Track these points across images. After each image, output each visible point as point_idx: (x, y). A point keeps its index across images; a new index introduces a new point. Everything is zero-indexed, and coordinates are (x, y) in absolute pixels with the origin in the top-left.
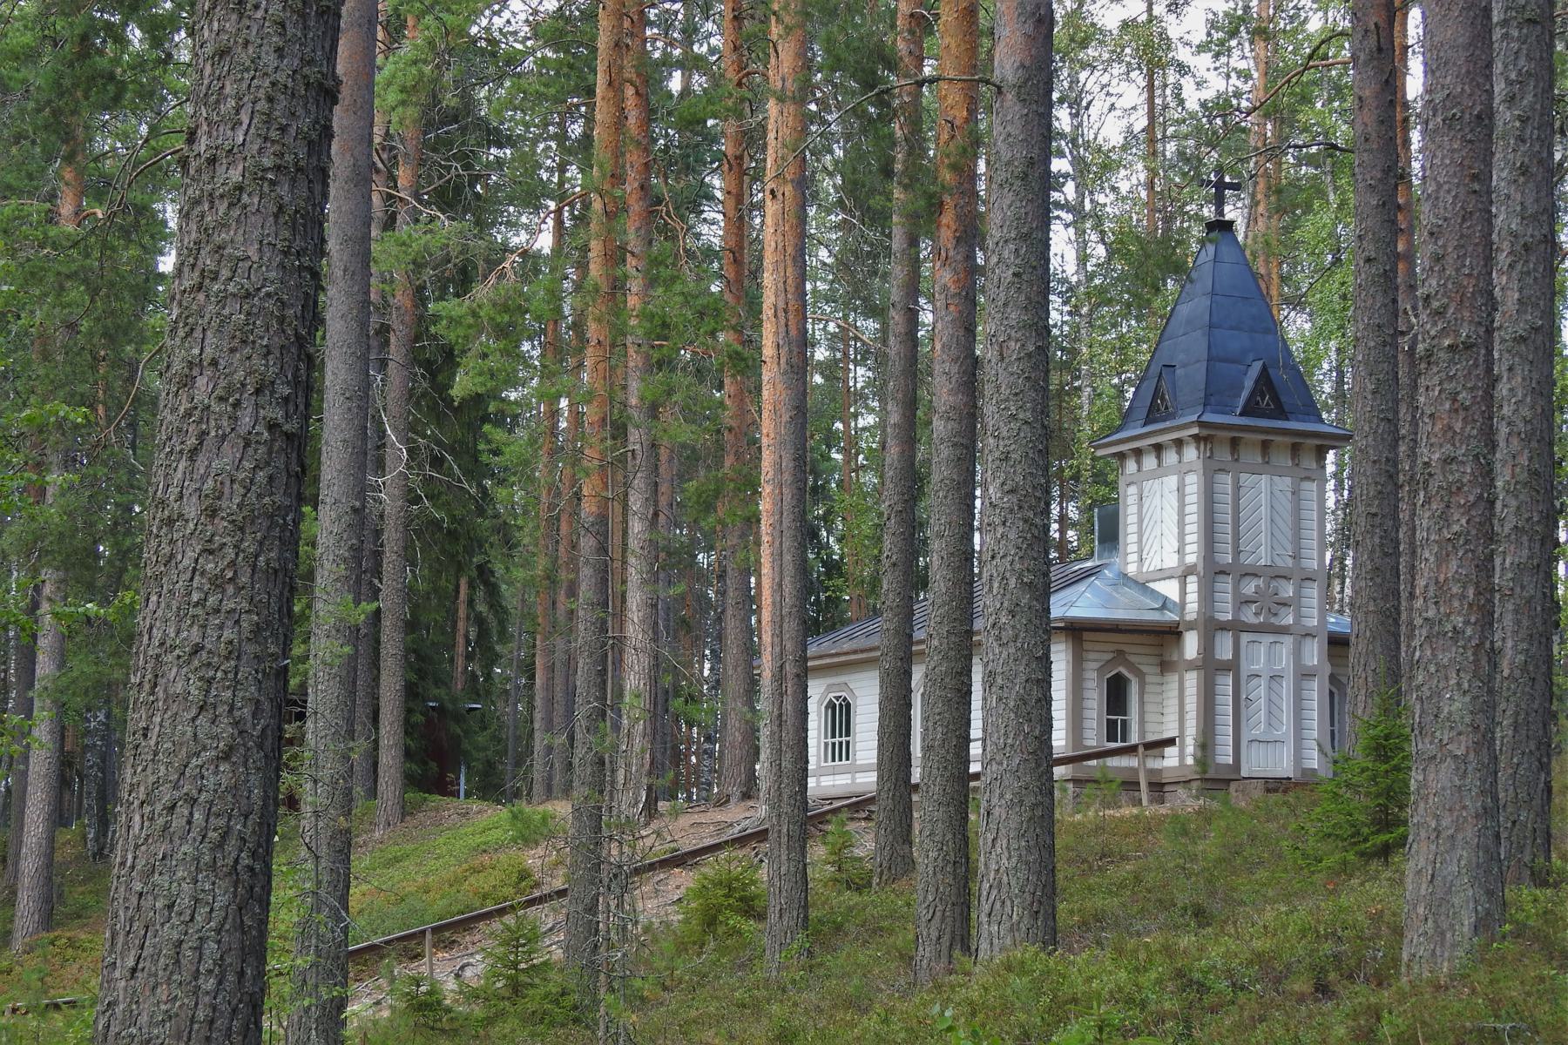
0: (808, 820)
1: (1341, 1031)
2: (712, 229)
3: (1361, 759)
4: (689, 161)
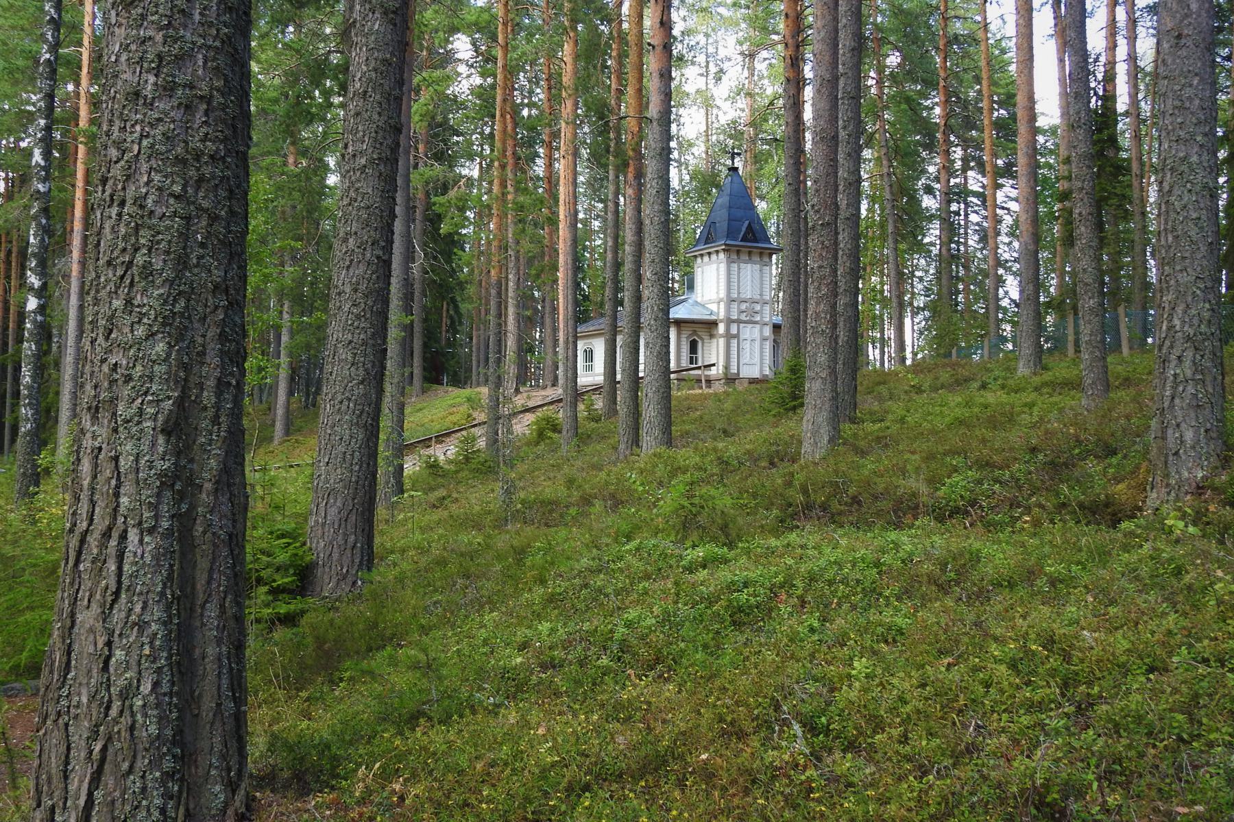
0: (576, 394)
1: (779, 481)
2: (539, 168)
3: (786, 374)
4: (531, 143)
